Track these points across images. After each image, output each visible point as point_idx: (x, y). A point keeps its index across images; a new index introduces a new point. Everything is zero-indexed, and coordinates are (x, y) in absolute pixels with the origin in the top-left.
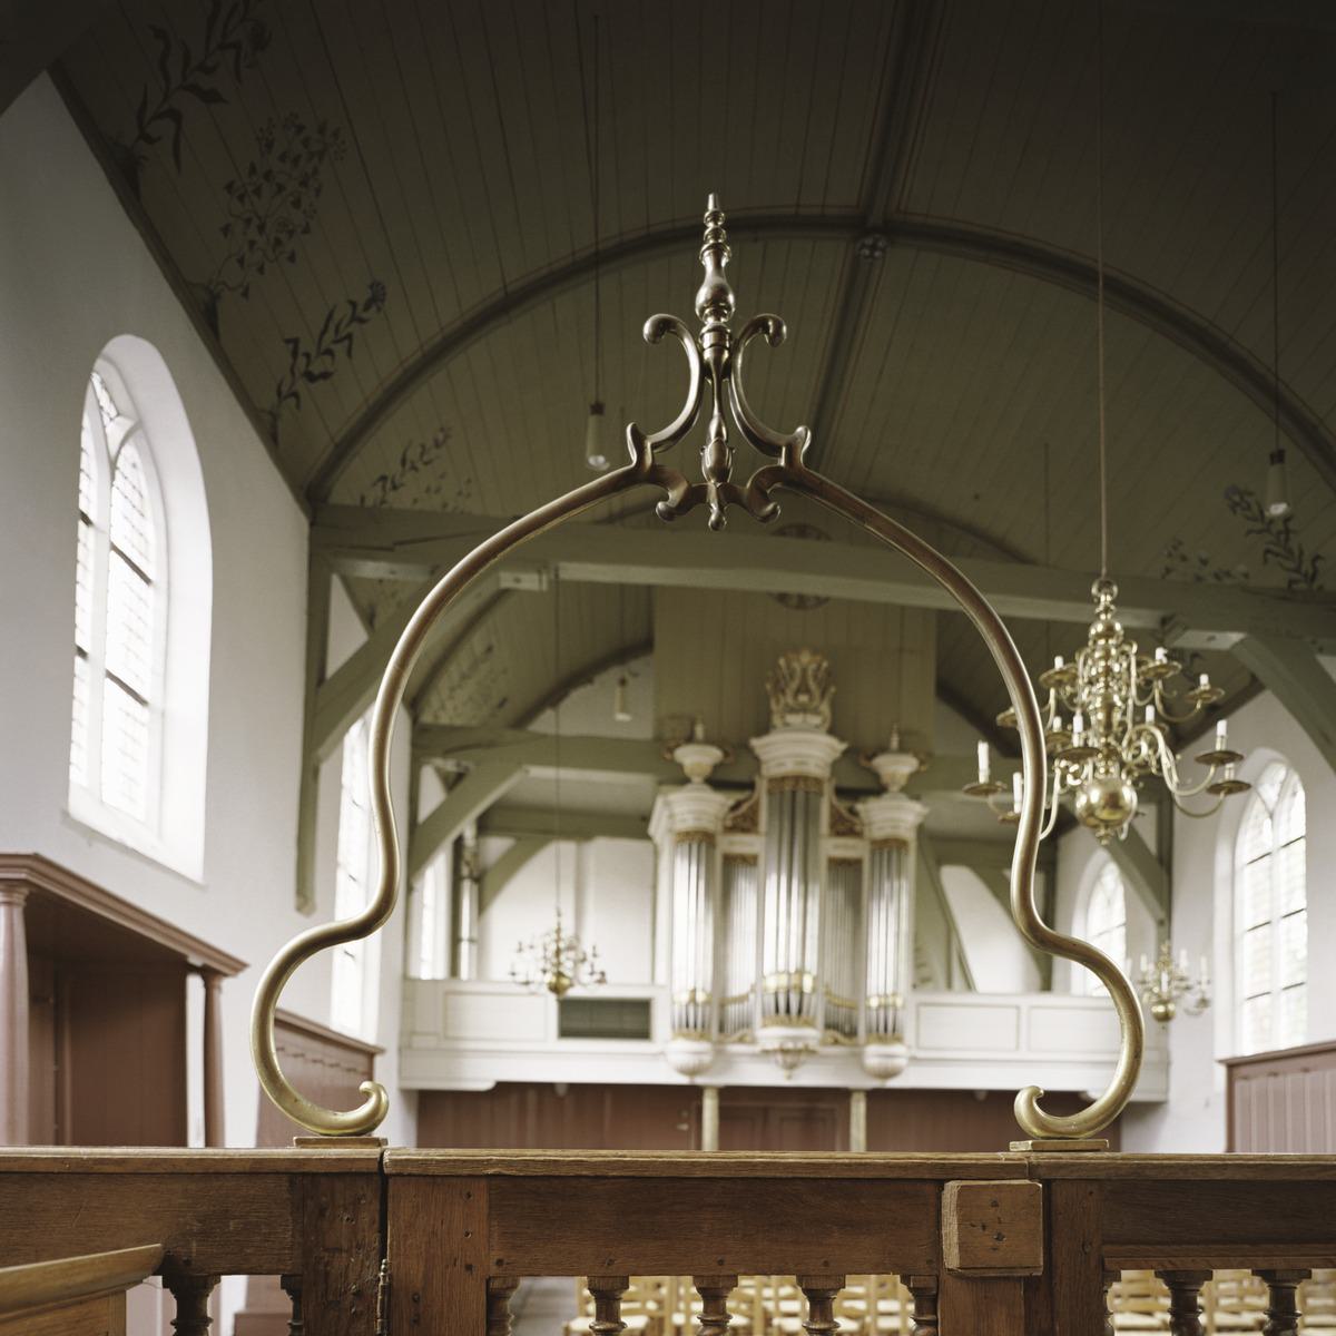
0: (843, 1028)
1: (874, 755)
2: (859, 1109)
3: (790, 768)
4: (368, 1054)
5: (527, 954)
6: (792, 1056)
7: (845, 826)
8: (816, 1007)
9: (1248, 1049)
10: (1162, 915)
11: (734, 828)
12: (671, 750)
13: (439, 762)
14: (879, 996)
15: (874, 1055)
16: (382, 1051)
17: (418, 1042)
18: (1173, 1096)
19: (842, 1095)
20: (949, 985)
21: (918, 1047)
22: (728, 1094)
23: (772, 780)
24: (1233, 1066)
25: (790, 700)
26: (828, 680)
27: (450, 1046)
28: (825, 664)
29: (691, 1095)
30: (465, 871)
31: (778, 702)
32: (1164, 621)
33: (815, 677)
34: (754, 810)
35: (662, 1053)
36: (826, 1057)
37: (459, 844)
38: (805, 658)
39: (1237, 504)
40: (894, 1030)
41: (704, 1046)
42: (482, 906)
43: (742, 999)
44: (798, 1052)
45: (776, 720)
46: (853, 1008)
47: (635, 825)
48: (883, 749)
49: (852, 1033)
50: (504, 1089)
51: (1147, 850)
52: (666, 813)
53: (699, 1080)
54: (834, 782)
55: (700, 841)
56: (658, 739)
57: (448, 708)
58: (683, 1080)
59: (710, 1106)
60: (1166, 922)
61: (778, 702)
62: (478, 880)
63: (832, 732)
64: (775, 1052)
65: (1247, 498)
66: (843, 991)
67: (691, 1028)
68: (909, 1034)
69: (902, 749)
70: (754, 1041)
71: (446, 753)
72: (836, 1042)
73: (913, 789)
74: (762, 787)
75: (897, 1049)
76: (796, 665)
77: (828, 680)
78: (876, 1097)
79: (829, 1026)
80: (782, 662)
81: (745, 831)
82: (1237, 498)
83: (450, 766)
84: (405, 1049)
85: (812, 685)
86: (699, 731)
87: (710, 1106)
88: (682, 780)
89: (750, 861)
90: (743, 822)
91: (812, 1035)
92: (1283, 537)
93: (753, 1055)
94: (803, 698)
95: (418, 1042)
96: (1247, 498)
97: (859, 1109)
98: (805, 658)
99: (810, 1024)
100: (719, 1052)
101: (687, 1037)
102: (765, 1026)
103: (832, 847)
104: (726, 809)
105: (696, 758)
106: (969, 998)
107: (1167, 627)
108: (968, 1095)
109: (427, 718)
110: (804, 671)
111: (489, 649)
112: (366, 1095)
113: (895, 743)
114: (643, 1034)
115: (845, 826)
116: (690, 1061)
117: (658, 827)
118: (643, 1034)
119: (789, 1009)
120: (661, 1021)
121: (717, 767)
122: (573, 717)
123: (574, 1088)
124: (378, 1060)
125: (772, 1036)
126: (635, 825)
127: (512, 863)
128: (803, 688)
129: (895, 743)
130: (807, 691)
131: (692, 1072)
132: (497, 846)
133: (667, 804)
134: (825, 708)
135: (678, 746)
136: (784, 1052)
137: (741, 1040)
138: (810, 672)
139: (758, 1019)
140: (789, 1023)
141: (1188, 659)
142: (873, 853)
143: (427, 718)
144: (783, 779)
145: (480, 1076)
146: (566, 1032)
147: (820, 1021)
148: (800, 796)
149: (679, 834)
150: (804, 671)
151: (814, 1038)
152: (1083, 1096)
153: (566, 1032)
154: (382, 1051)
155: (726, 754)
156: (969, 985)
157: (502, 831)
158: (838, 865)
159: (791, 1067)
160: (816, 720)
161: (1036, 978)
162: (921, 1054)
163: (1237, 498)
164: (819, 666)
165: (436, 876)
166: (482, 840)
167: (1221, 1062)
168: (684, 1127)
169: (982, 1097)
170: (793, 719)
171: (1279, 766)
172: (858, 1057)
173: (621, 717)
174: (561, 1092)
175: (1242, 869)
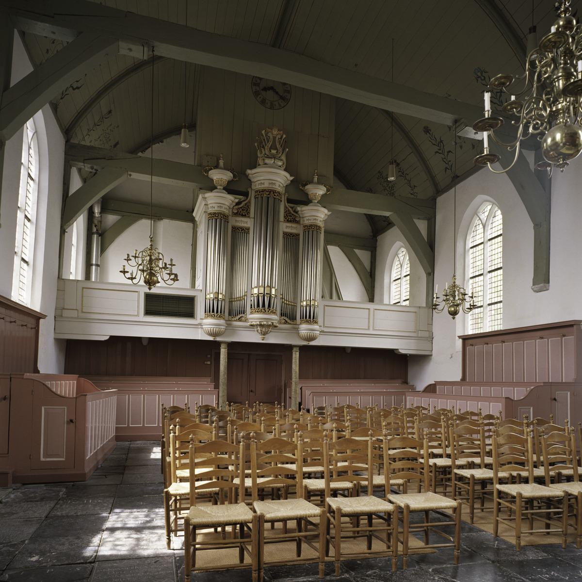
0: (289, 316)
1: (306, 184)
2: (296, 355)
3: (266, 185)
4: (36, 317)
5: (133, 262)
6: (265, 328)
7: (292, 217)
8: (277, 304)
9: (470, 332)
10: (430, 271)
11: (236, 214)
12: (207, 172)
13: (81, 165)
14: (306, 300)
15: (304, 329)
16: (44, 317)
17: (66, 313)
18: (434, 353)
19: (289, 348)
20: (331, 297)
21: (324, 326)
22: (232, 346)
23: (256, 192)
24: (465, 339)
25: (267, 152)
26: (285, 144)
27: (85, 316)
28: (284, 136)
29: (216, 345)
30: (95, 230)
31: (261, 153)
32: (456, 121)
33: (280, 142)
34: (248, 206)
35: (200, 324)
36: (280, 329)
37: (91, 212)
38: (275, 132)
39: (479, 77)
40: (314, 318)
41: (222, 322)
42: (103, 249)
43: (240, 299)
44: (269, 326)
45: (260, 161)
46: (295, 306)
47: (186, 215)
48: (311, 182)
49: (293, 318)
50: (114, 340)
51: (425, 240)
52: (204, 203)
53: (218, 339)
54: (286, 195)
55: (218, 218)
56: (200, 165)
57: (88, 137)
58: (211, 338)
59: (223, 352)
60: (432, 274)
61: (261, 153)
62: (101, 235)
63: (286, 170)
64: (257, 325)
65: (484, 74)
66: (290, 297)
67: (212, 311)
68: (320, 320)
69: (319, 183)
70: (246, 321)
71: (85, 161)
72: (286, 322)
73: (324, 201)
74: (252, 195)
75: (316, 327)
76: (270, 134)
77: (285, 144)
78: (302, 349)
79: (281, 315)
80: (263, 132)
81: (243, 216)
82: (479, 74)
83: (87, 168)
84: (58, 317)
85: (278, 146)
86: (221, 162)
87: (223, 352)
88: (212, 188)
89: (246, 231)
90: (241, 211)
91: (275, 318)
92: (499, 94)
93: (246, 327)
94: (274, 152)
95: (66, 313)
96: (484, 74)
97: (296, 355)
98: (275, 132)
99: (274, 313)
100: (229, 325)
101: (213, 317)
102: (252, 313)
103: (285, 227)
104: (234, 204)
105: (219, 176)
106: (339, 304)
107: (457, 125)
108: (343, 349)
109: (74, 141)
110: (274, 138)
111: (110, 112)
112: (537, 420)
113: (316, 179)
114: (191, 314)
115: (292, 217)
116: (216, 329)
117: (199, 214)
118: (191, 314)
119: (263, 304)
120: (200, 309)
121: (229, 182)
122: (158, 151)
123: (151, 340)
124: (41, 321)
125: (255, 317)
126: (186, 215)
127: (119, 228)
128: (273, 147)
129: (316, 179)
130: (276, 149)
131: (214, 335)
132: (111, 219)
133: (205, 198)
134: (283, 158)
135: (211, 169)
136: (261, 325)
137: (240, 320)
138: (277, 138)
139: (248, 309)
140: (265, 312)
141: (446, 154)
142: (304, 232)
143: (74, 141)
144: (263, 191)
145: (102, 332)
146: (148, 312)
147: (278, 312)
148: (271, 201)
149: (210, 214)
150: (274, 138)
151: (276, 320)
152: (396, 352)
153: (148, 312)
154: (44, 317)
155: (234, 176)
156: (339, 297)
157: (114, 211)
158: (287, 235)
159: (265, 334)
160: (280, 163)
161: (366, 298)
162: (326, 330)
163: (479, 74)
164: (282, 137)
165: (78, 229)
166: (104, 215)
167: (459, 337)
168: (209, 363)
169: (349, 351)
170: (270, 161)
171: (488, 203)
172: (296, 330)
173: (183, 145)
174: (145, 343)
175: (469, 250)
